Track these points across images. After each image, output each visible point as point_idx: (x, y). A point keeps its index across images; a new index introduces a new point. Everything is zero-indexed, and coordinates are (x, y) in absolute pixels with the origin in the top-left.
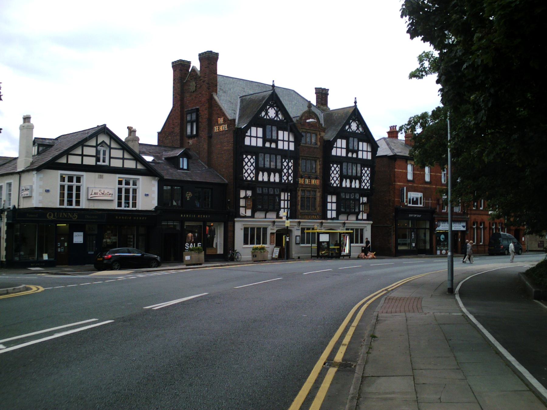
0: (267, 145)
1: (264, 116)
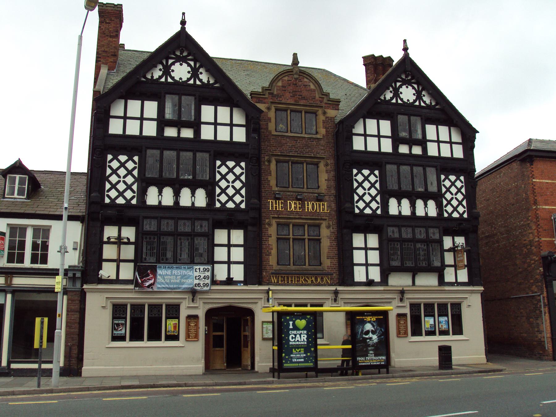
0: (403, 149)
1: (392, 99)
